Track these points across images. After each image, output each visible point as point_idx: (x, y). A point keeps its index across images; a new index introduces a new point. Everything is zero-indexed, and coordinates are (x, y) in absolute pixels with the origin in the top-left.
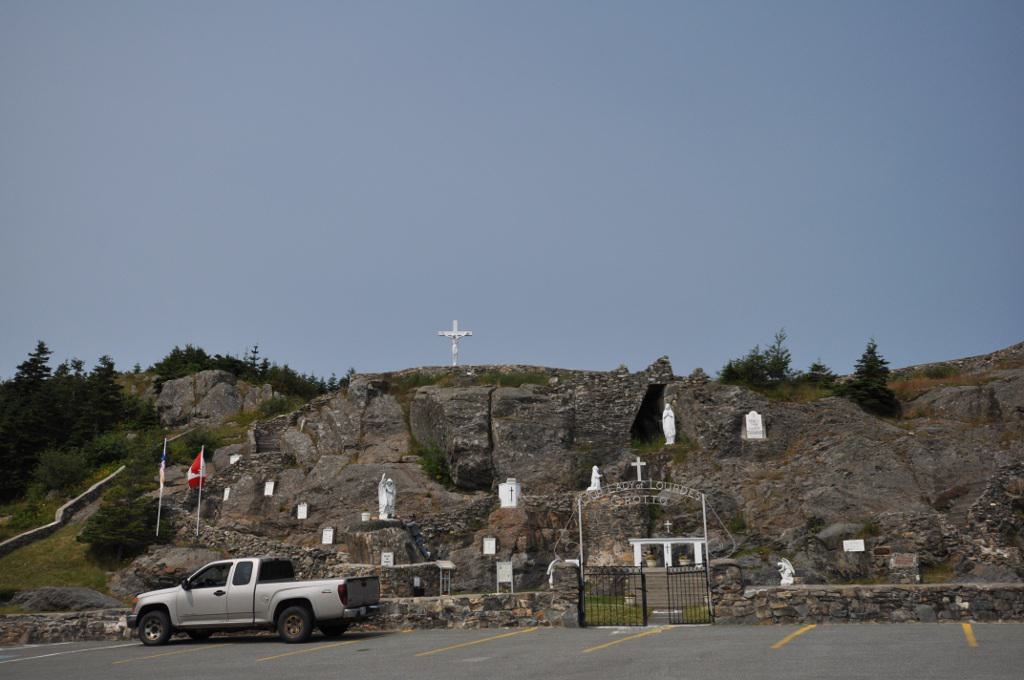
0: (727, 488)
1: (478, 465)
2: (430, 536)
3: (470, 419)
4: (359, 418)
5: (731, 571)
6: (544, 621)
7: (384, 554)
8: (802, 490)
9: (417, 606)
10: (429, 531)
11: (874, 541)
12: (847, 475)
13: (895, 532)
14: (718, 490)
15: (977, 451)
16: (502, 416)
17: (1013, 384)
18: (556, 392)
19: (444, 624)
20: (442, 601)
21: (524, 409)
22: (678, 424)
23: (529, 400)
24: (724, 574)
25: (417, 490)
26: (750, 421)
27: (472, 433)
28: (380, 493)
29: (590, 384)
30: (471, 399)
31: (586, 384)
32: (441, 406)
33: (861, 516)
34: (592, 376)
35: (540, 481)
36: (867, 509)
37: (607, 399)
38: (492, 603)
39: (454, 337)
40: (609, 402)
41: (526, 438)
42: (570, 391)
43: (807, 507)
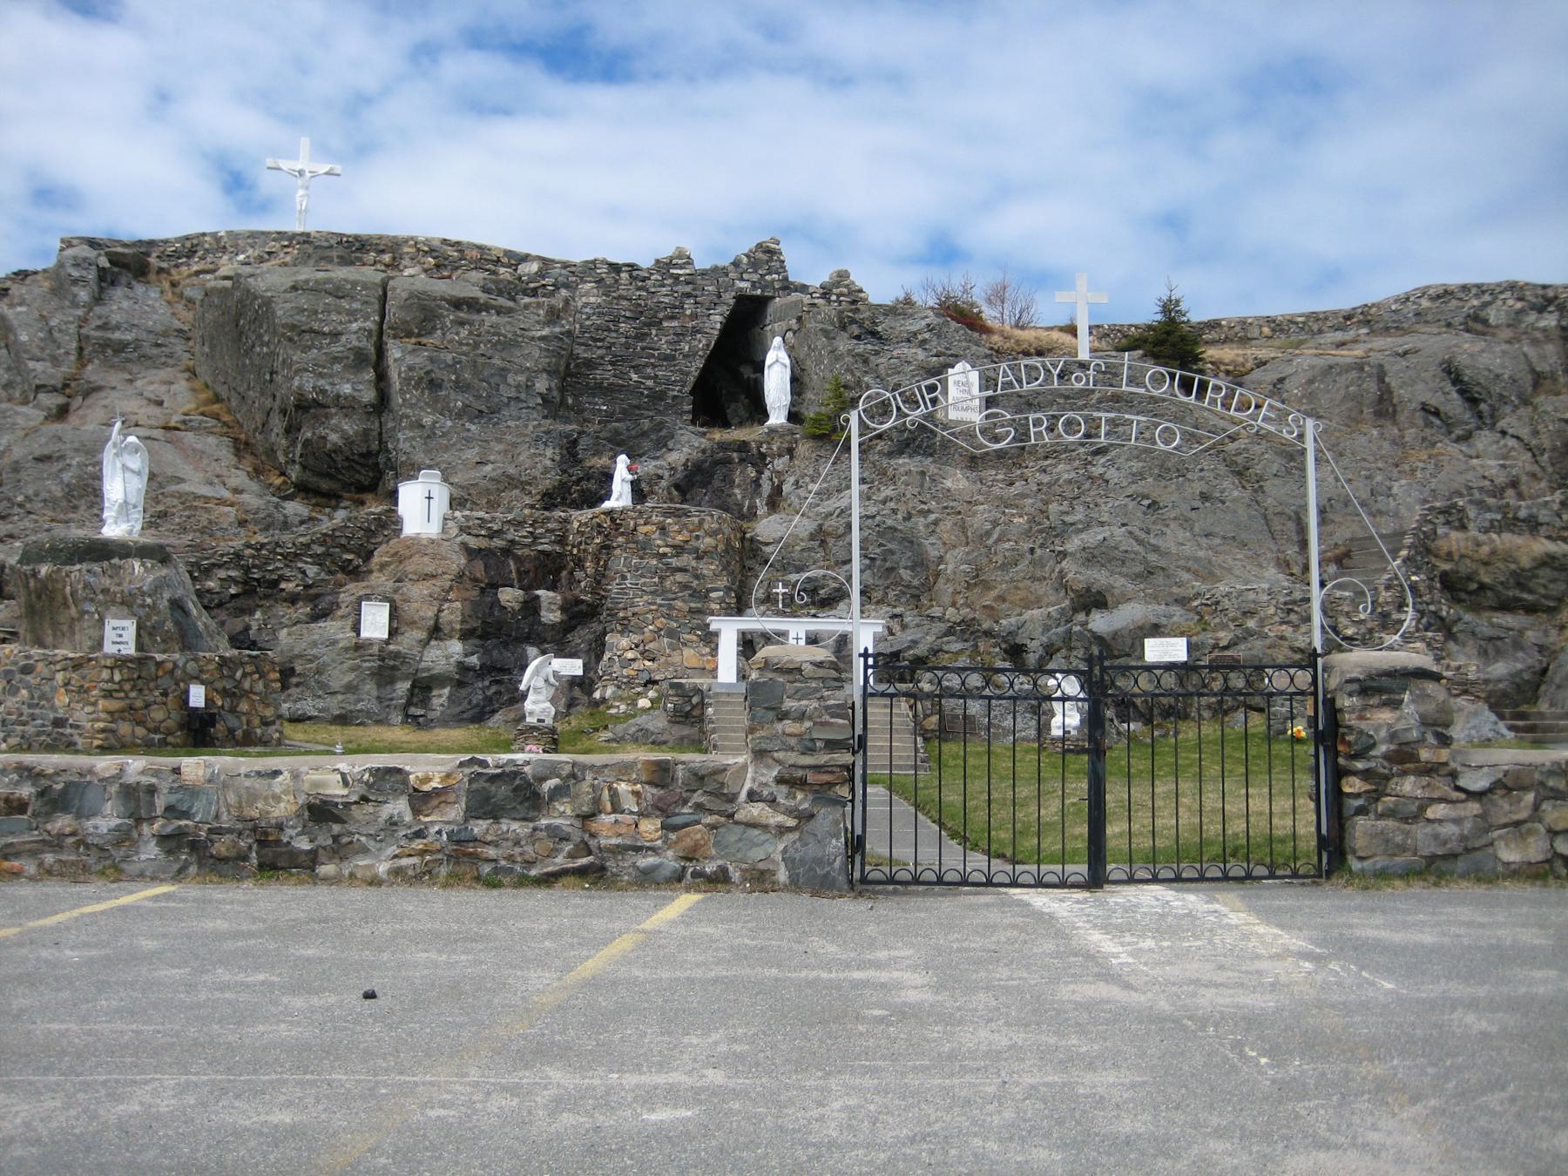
0: (908, 517)
1: (349, 442)
2: (233, 591)
3: (336, 335)
4: (72, 328)
5: (1424, 697)
6: (710, 868)
7: (111, 623)
8: (1063, 530)
9: (193, 792)
10: (231, 579)
11: (1212, 642)
12: (1149, 506)
13: (1251, 624)
14: (889, 522)
15: (1367, 478)
16: (409, 335)
17: (1413, 359)
18: (534, 293)
19: (305, 866)
20: (296, 776)
21: (462, 323)
22: (798, 383)
23: (472, 305)
24: (1396, 705)
25: (205, 490)
26: (957, 383)
27: (337, 367)
28: (107, 471)
29: (609, 281)
30: (338, 292)
31: (600, 281)
32: (268, 303)
33: (1175, 590)
34: (615, 268)
35: (492, 487)
36: (1186, 576)
37: (648, 319)
38: (503, 790)
39: (301, 173)
40: (649, 325)
41: (460, 386)
42: (564, 292)
43: (1074, 568)
